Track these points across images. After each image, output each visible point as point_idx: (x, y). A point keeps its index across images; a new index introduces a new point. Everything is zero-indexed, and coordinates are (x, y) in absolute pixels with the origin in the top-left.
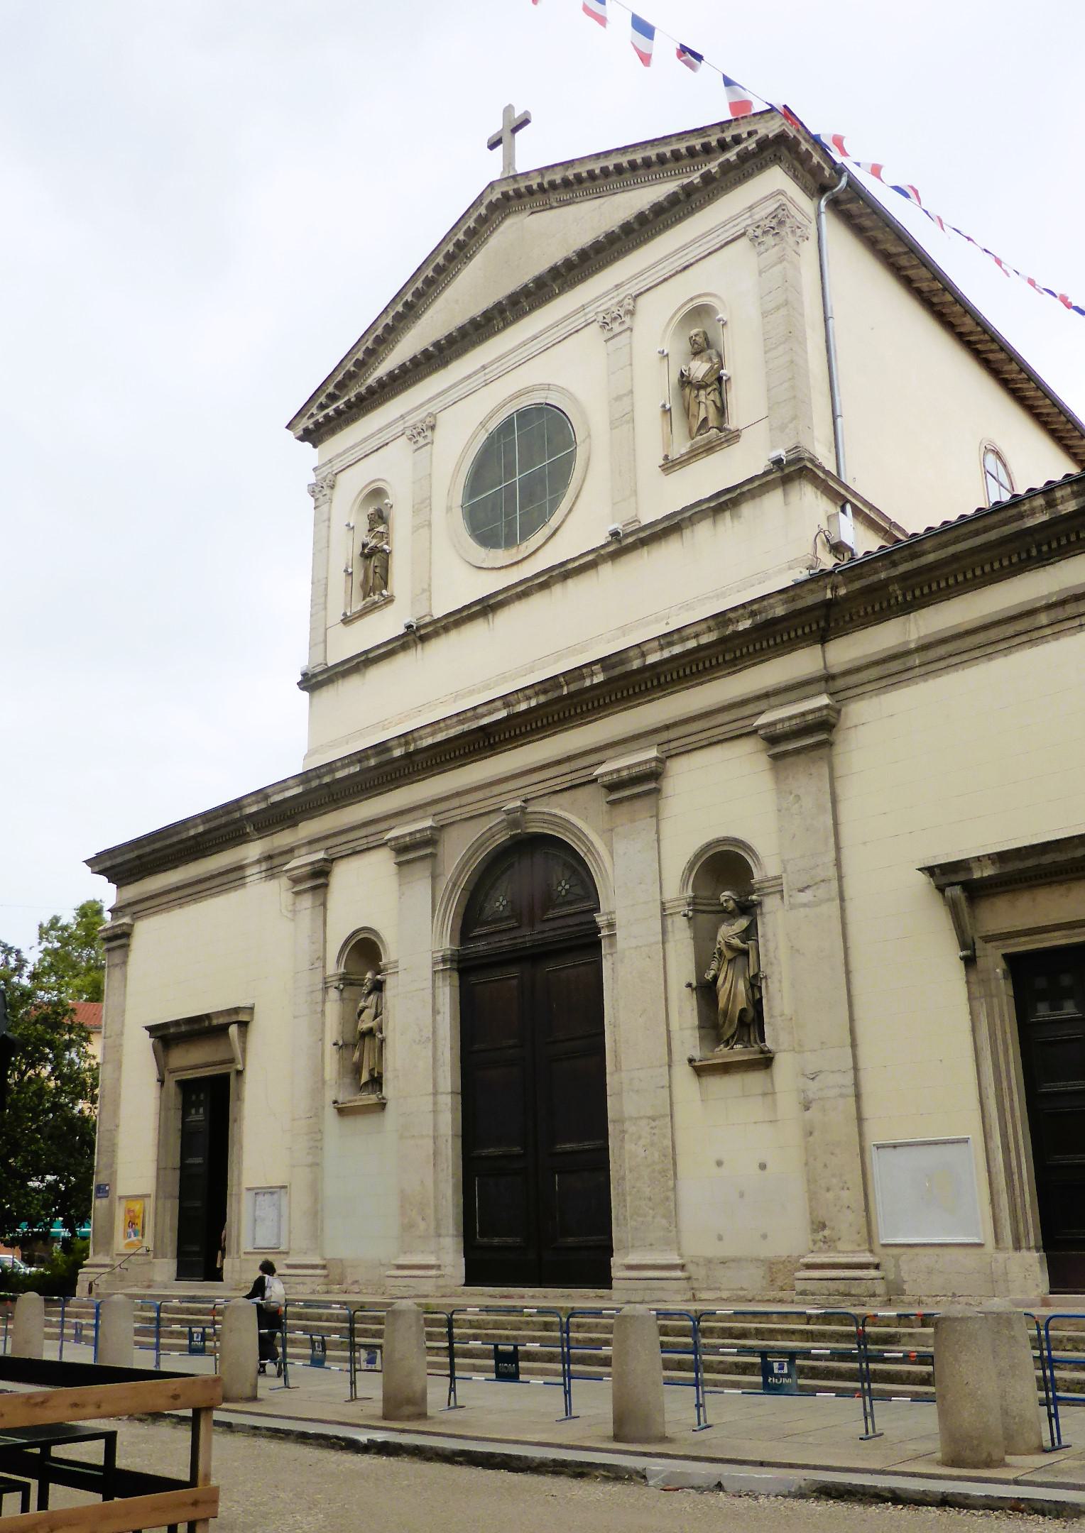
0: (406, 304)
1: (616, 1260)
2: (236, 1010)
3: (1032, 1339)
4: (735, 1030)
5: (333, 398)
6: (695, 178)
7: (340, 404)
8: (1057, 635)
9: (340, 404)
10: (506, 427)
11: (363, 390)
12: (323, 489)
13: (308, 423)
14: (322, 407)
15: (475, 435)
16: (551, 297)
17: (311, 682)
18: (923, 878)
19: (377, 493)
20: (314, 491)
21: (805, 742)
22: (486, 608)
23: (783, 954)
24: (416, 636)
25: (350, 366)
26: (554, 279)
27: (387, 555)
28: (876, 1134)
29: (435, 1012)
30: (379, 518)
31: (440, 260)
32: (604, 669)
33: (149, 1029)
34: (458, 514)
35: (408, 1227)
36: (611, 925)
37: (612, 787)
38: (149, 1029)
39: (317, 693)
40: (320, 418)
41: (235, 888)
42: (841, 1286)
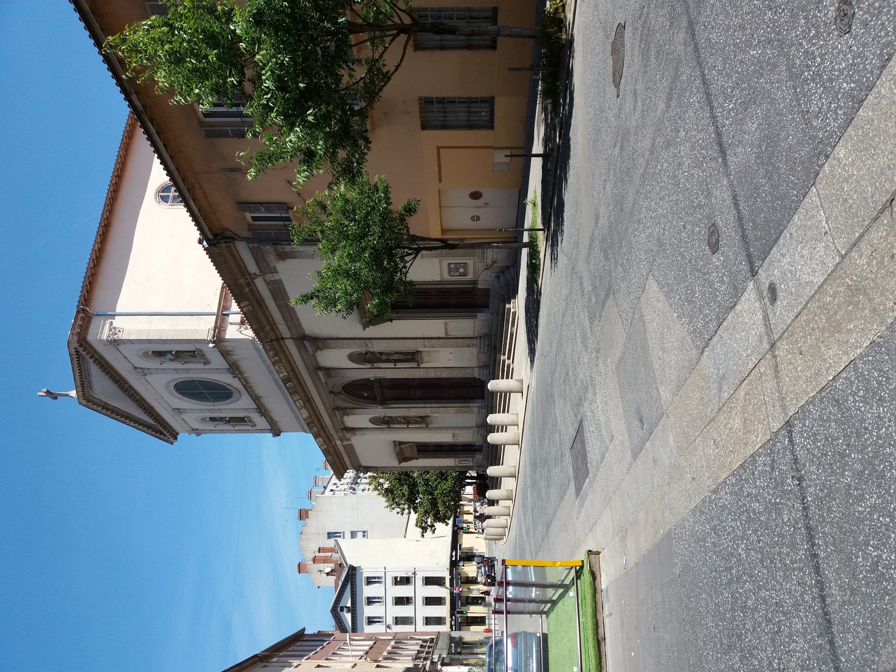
2: (395, 446)
4: (412, 357)
5: (161, 433)
6: (84, 353)
9: (163, 430)
10: (182, 394)
12: (198, 432)
13: (172, 439)
14: (165, 435)
16: (130, 386)
25: (150, 431)
27: (177, 352)
28: (443, 335)
30: (213, 419)
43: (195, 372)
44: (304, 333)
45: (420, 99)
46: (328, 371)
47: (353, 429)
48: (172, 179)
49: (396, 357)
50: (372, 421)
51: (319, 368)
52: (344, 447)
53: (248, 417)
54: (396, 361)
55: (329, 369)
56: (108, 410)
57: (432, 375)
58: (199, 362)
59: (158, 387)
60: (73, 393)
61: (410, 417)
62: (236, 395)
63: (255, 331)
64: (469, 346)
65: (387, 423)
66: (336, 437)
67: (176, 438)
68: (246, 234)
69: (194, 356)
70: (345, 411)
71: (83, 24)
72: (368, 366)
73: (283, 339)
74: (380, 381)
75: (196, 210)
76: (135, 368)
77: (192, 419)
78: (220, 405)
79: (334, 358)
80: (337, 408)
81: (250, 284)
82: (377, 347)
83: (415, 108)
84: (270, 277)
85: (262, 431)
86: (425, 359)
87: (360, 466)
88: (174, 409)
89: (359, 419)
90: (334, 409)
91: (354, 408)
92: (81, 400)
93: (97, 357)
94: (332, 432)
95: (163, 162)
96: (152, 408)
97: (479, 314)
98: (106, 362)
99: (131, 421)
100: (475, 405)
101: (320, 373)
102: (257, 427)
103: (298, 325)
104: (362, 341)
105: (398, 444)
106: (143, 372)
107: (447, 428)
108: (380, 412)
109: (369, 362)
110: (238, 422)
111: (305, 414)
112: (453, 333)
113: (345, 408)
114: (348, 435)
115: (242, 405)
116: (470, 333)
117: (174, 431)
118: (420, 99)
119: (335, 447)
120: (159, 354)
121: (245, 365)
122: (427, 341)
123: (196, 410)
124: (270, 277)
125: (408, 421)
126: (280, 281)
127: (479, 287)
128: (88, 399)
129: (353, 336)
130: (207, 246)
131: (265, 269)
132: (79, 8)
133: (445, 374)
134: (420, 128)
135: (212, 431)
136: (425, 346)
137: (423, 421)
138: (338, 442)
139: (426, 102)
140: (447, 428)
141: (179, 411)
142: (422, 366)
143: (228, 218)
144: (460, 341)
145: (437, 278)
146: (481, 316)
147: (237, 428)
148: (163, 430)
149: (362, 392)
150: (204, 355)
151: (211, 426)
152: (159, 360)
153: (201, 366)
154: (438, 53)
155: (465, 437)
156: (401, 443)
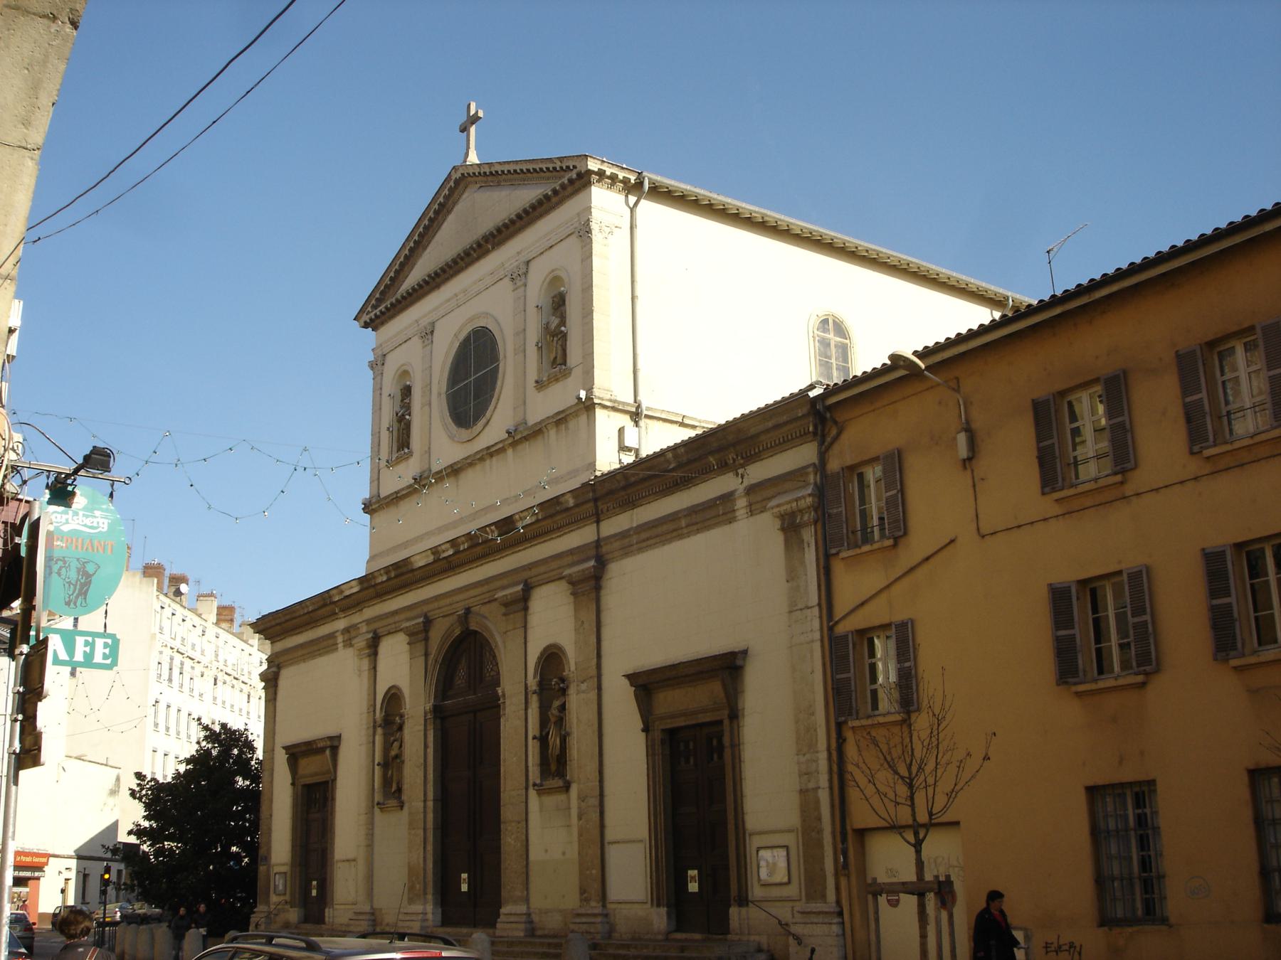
0: (415, 242)
1: (503, 910)
2: (331, 738)
3: (216, 933)
4: (554, 765)
5: (379, 301)
6: (565, 181)
7: (382, 308)
8: (640, 550)
9: (382, 308)
10: (467, 339)
11: (393, 300)
12: (377, 365)
13: (366, 318)
14: (375, 307)
15: (452, 343)
16: (487, 252)
17: (368, 508)
18: (626, 682)
19: (405, 373)
20: (372, 366)
21: (589, 585)
22: (455, 471)
23: (575, 721)
24: (421, 482)
25: (387, 281)
26: (487, 241)
27: (564, 336)
28: (610, 835)
29: (426, 746)
30: (407, 391)
31: (431, 214)
32: (452, 546)
33: (628, 677)
34: (444, 397)
35: (412, 888)
36: (504, 695)
37: (506, 605)
38: (628, 677)
39: (376, 515)
40: (372, 315)
41: (327, 652)
42: (584, 927)
43: (518, 365)
44: (612, 560)
45: (1152, 783)
46: (521, 603)
47: (375, 654)
48: (858, 381)
49: (554, 740)
50: (393, 697)
51: (528, 589)
52: (332, 636)
53: (411, 454)
54: (543, 740)
55: (526, 609)
56: (437, 213)
57: (508, 812)
58: (540, 371)
59: (486, 298)
60: (473, 158)
61: (400, 770)
62: (465, 434)
63: (612, 475)
64: (583, 891)
65: (389, 715)
66: (356, 618)
67: (366, 326)
68: (834, 465)
69: (554, 363)
70: (420, 634)
71: (975, 327)
72: (533, 683)
73: (598, 522)
74: (493, 706)
75: (1099, 294)
76: (528, 263)
77: (409, 356)
78: (440, 407)
79: (552, 619)
80: (428, 622)
81: (724, 467)
82: (578, 703)
83: (1128, 774)
84: (741, 503)
85: (376, 479)
86: (551, 800)
87: (279, 667)
88: (433, 324)
89: (399, 665)
90: (426, 616)
91: (426, 655)
92: (461, 171)
93: (554, 200)
94: (370, 612)
95: (983, 330)
96: (438, 286)
97: (663, 910)
98: (541, 216)
99: (411, 250)
100: (430, 908)
101: (520, 587)
102: (384, 472)
103: (627, 552)
104: (594, 672)
105: (333, 745)
106: (519, 276)
107: (370, 846)
108: (417, 706)
109: (540, 684)
110: (401, 436)
111: (420, 562)
112: (613, 854)
113: (426, 639)
114: (360, 642)
115: (439, 442)
116: (614, 893)
117: (382, 324)
118: (1152, 783)
119: (332, 616)
120: (559, 303)
121: (532, 454)
122: (595, 802)
123: (432, 367)
124: (741, 503)
125: (390, 764)
126: (731, 520)
127: (734, 911)
128: (459, 183)
129: (603, 653)
130: (812, 394)
131: (759, 494)
132: (1264, 216)
133: (509, 841)
134: (1091, 783)
135: (378, 389)
136: (582, 798)
137: (389, 788)
138: (340, 624)
139: (1142, 792)
140: (370, 846)
141: (428, 334)
142: (532, 793)
143: (862, 436)
144: (595, 872)
145: (751, 823)
146: (659, 919)
147: (385, 436)
148: (382, 307)
149: (463, 664)
150: (557, 380)
151: (390, 386)
152: (546, 302)
153: (532, 375)
154: (1247, 814)
155: (346, 887)
156: (335, 749)
